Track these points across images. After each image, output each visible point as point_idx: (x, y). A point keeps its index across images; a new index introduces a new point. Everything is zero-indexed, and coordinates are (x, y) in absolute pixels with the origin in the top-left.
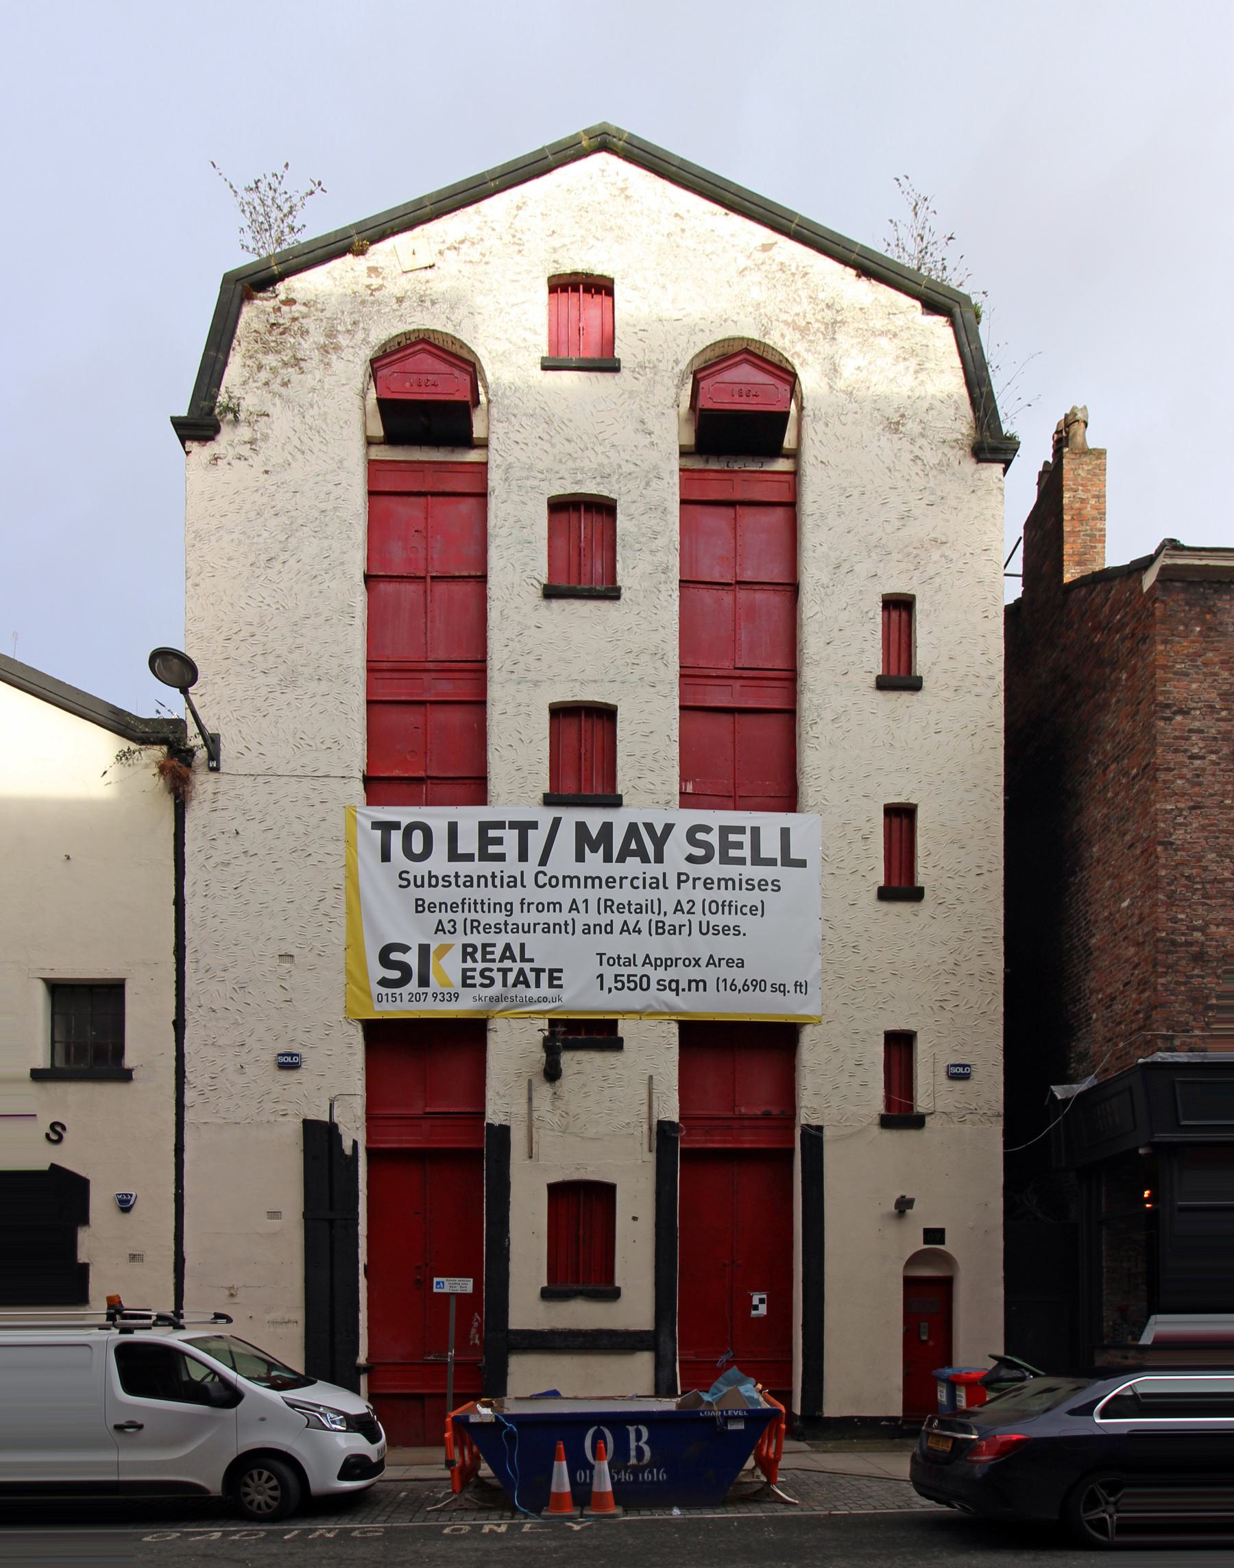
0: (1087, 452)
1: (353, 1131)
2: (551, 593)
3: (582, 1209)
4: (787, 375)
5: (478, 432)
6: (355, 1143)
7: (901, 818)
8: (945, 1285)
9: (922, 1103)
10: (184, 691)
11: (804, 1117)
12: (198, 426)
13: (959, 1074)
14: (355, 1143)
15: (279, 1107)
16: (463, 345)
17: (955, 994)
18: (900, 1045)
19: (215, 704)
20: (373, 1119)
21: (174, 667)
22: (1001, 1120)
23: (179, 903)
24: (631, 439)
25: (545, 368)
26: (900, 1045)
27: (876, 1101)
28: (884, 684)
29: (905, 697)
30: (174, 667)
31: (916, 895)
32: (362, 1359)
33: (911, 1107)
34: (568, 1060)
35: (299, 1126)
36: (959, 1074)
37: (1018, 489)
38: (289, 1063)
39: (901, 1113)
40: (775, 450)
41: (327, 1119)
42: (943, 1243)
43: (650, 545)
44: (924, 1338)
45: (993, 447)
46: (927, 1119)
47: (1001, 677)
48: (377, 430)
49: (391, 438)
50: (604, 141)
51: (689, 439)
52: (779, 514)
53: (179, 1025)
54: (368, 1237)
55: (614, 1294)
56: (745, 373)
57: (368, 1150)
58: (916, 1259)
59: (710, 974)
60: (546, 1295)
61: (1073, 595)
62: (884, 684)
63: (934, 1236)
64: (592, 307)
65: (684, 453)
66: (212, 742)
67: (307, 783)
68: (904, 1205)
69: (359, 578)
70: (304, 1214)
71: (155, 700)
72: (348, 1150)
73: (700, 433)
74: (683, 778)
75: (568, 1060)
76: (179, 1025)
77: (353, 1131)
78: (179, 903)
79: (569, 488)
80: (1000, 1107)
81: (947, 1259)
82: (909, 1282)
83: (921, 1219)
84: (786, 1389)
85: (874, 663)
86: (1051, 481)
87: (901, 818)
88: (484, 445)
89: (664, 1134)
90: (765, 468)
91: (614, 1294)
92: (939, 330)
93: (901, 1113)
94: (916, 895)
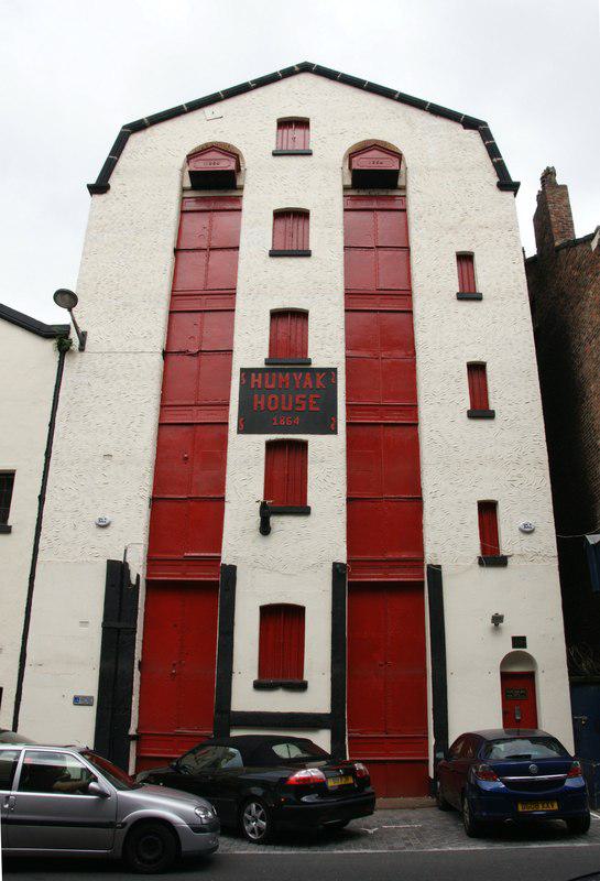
0: (558, 187)
1: (137, 568)
2: (274, 254)
3: (282, 622)
4: (399, 156)
5: (239, 183)
6: (138, 576)
7: (477, 370)
8: (529, 679)
9: (504, 549)
10: (70, 310)
11: (429, 559)
12: (99, 187)
13: (528, 531)
14: (138, 576)
15: (94, 551)
16: (234, 147)
17: (519, 476)
18: (488, 510)
19: (85, 316)
20: (152, 561)
21: (66, 299)
22: (557, 559)
23: (52, 425)
24: (320, 186)
25: (274, 154)
26: (488, 510)
27: (474, 546)
28: (461, 297)
29: (474, 304)
30: (66, 299)
31: (490, 415)
32: (132, 731)
33: (498, 551)
34: (275, 521)
35: (331, 567)
36: (528, 531)
37: (526, 204)
38: (103, 525)
39: (492, 556)
40: (395, 186)
41: (122, 560)
42: (524, 646)
43: (328, 233)
44: (518, 718)
45: (507, 185)
46: (509, 560)
47: (526, 293)
48: (188, 184)
49: (194, 187)
50: (306, 68)
51: (349, 182)
52: (401, 253)
53: (42, 499)
54: (143, 641)
55: (302, 687)
56: (375, 154)
57: (147, 581)
58: (508, 660)
59: (299, 330)
60: (258, 686)
61: (561, 252)
62: (461, 297)
63: (519, 642)
64: (298, 133)
65: (345, 188)
66: (83, 336)
67: (131, 355)
68: (497, 620)
69: (172, 250)
70: (103, 624)
71: (56, 316)
72: (134, 582)
73: (354, 179)
74: (347, 348)
75: (275, 521)
76: (42, 499)
77: (137, 568)
78: (52, 425)
79: (284, 206)
80: (556, 553)
81: (529, 659)
82: (505, 677)
83: (512, 628)
84: (414, 556)
85: (454, 286)
86: (542, 199)
87: (477, 370)
88: (242, 188)
89: (338, 570)
90: (390, 194)
91: (302, 687)
92: (473, 137)
93: (492, 556)
94: (490, 415)
